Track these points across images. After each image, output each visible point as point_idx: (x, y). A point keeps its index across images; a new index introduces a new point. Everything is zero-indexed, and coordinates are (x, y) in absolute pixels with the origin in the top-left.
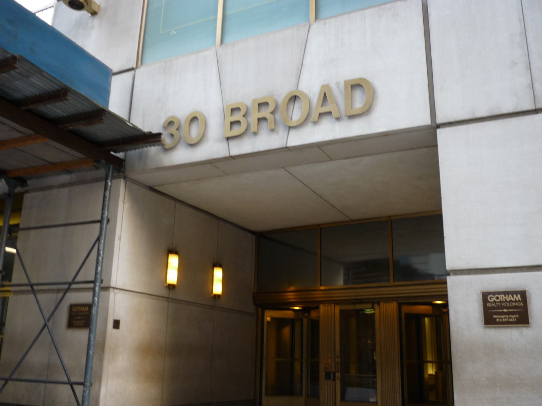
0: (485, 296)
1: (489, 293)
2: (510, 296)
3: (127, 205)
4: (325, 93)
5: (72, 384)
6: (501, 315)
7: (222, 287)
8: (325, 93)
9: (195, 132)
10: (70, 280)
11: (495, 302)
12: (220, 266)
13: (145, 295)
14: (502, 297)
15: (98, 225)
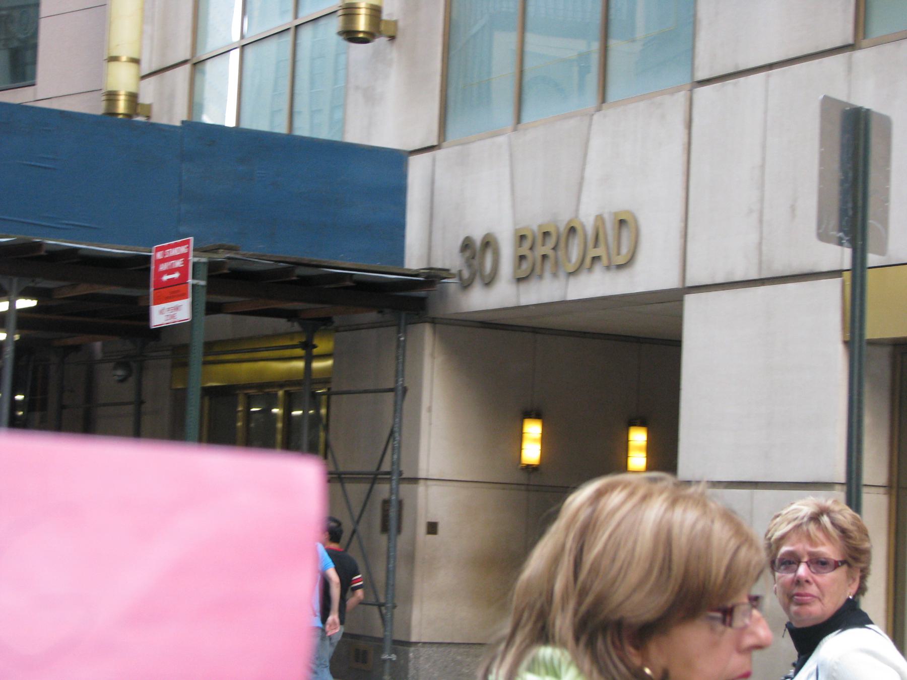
3: (439, 360)
15: (391, 395)
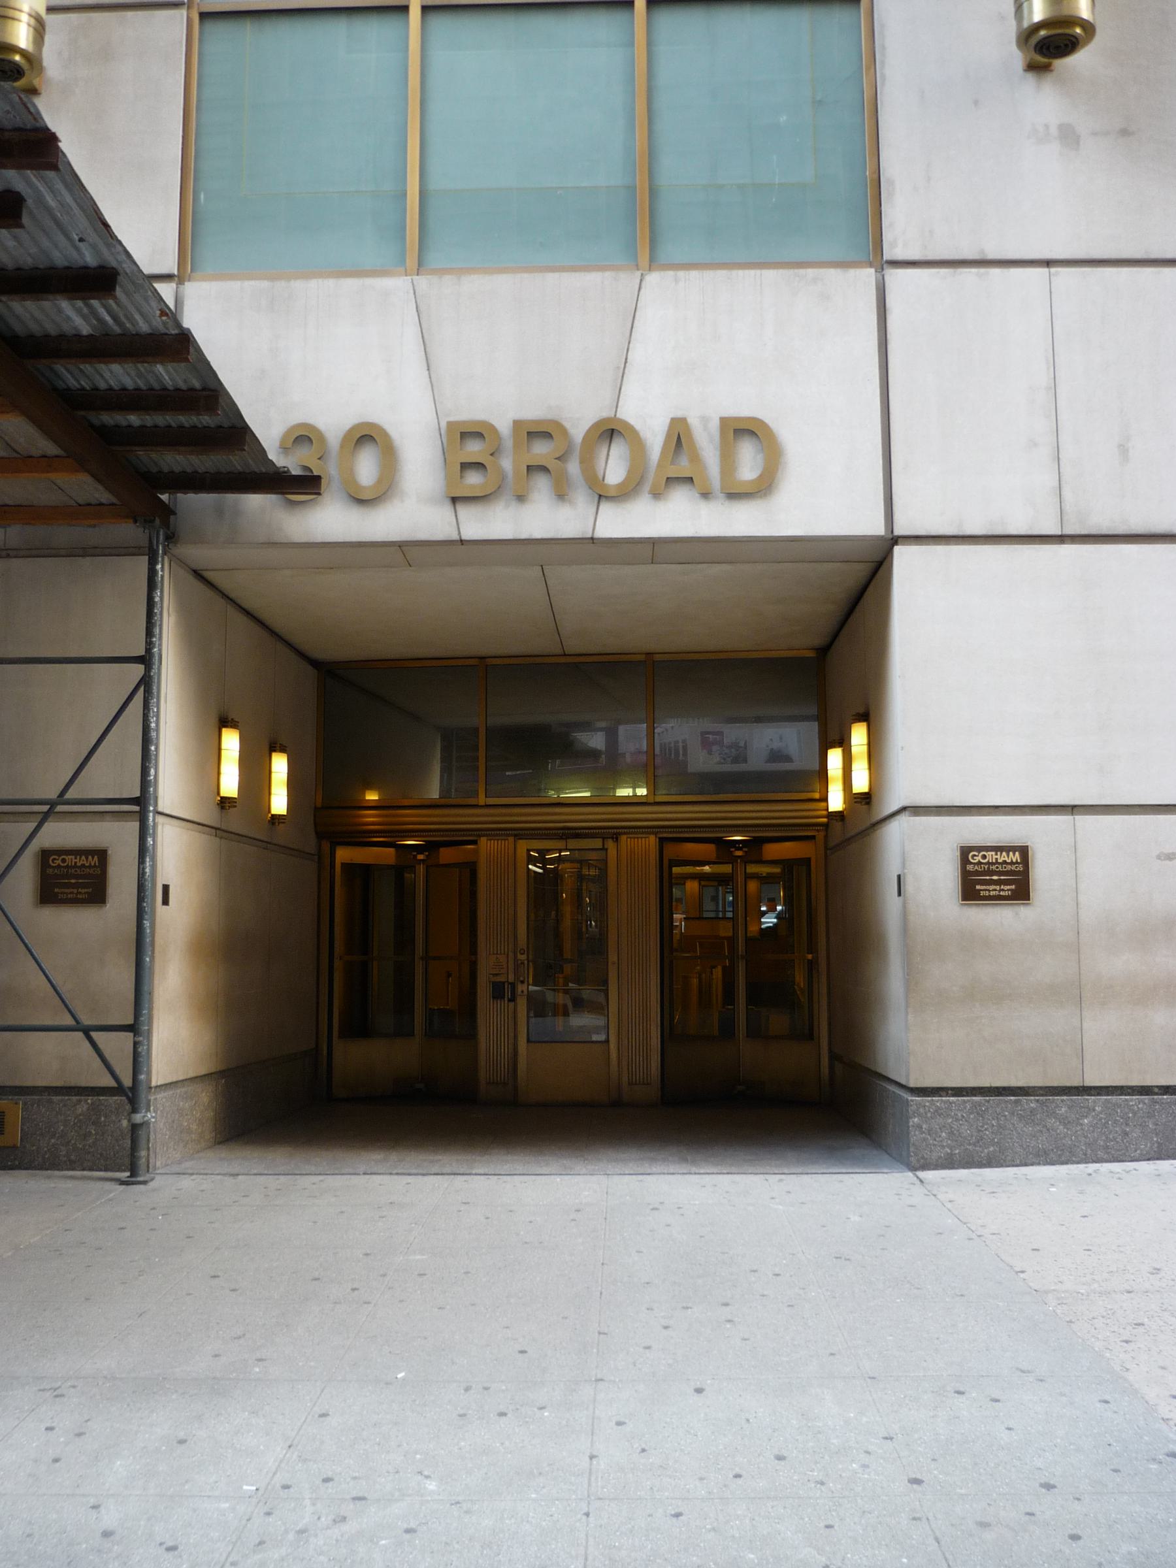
0: (965, 852)
1: (971, 849)
2: (1004, 854)
3: (173, 619)
4: (679, 434)
5: (87, 1031)
6: (989, 885)
7: (288, 796)
8: (679, 434)
9: (366, 468)
10: (53, 795)
11: (980, 863)
12: (282, 750)
13: (184, 823)
14: (991, 856)
